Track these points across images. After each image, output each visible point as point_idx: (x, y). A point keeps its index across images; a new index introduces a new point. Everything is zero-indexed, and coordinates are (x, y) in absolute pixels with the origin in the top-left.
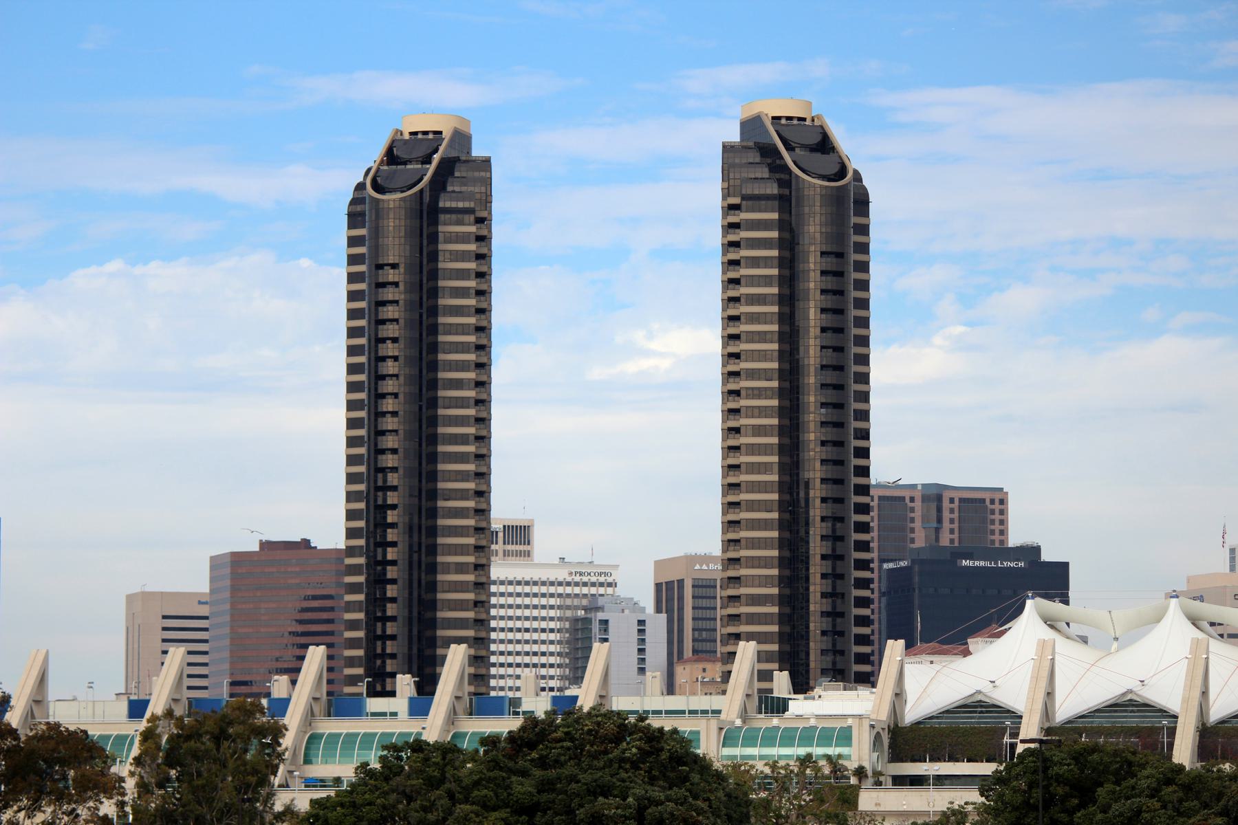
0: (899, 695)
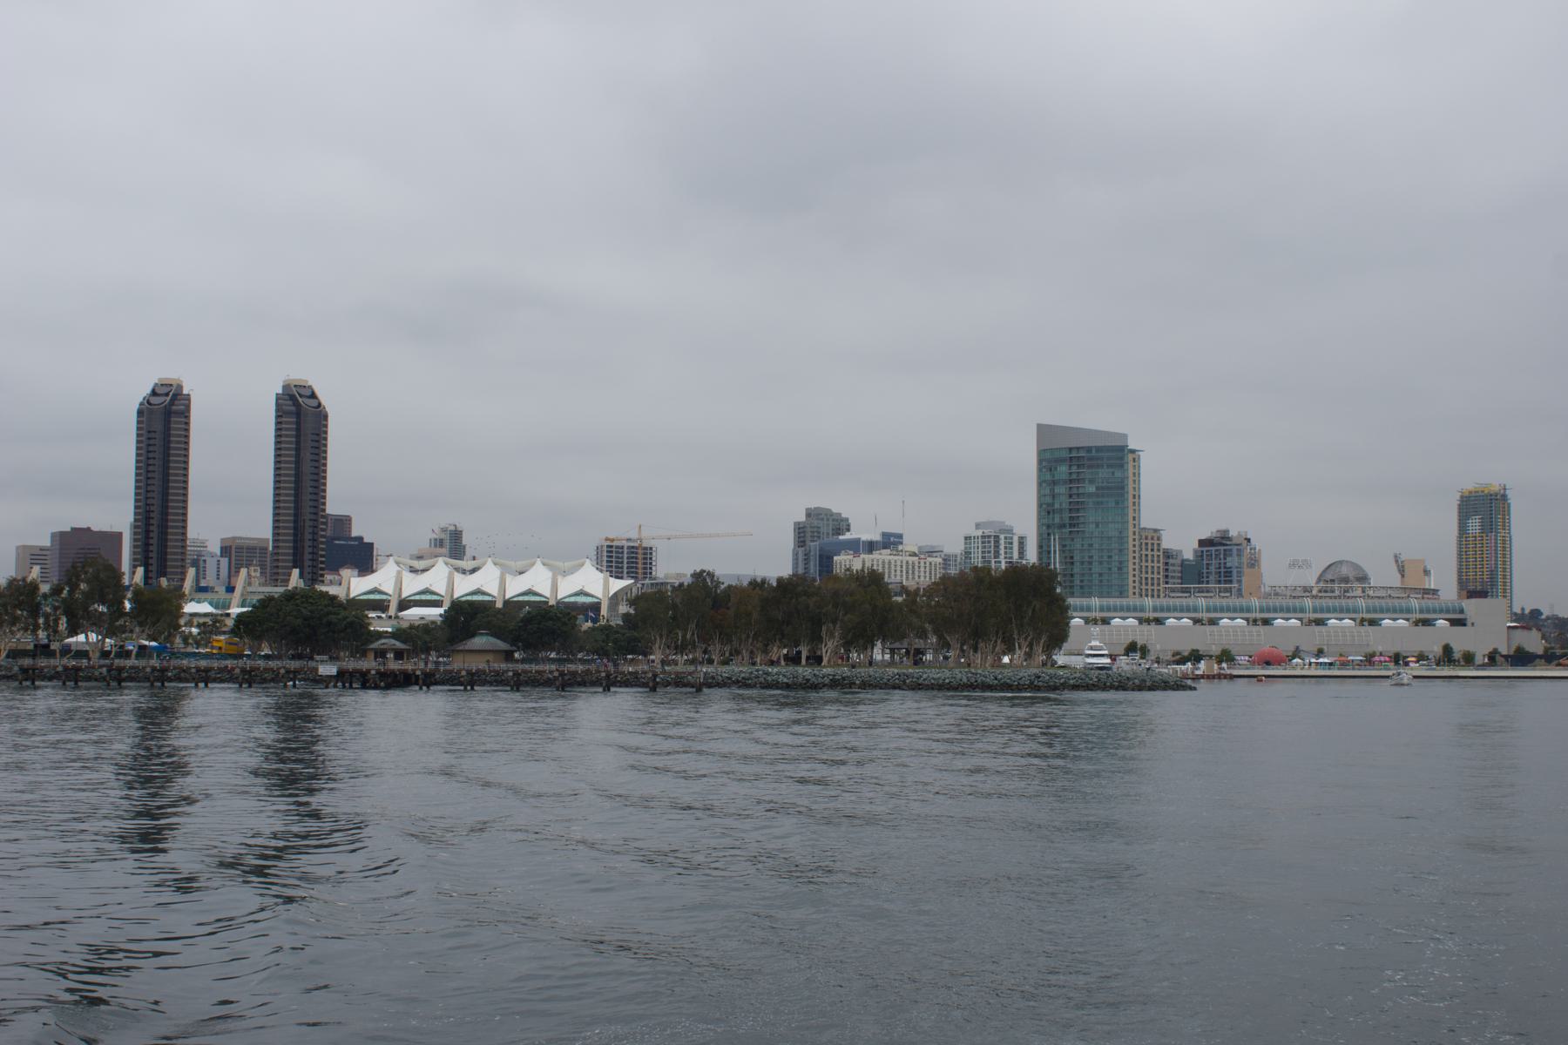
0: (349, 588)
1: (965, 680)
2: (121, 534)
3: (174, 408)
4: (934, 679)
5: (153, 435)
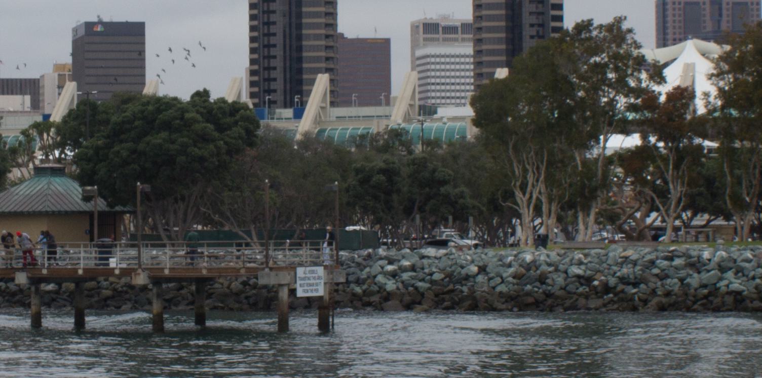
2: (385, 44)
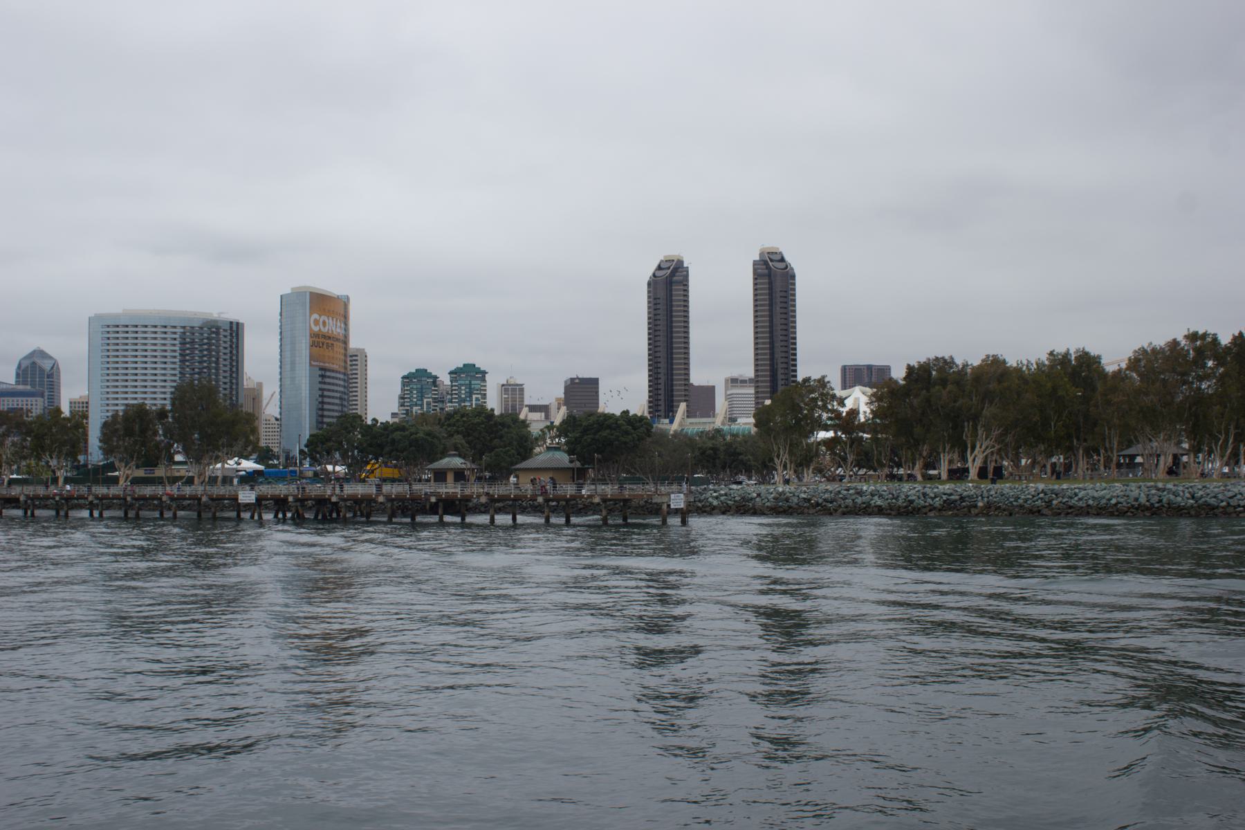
1: (1143, 500)
3: (675, 278)
4: (1094, 498)
5: (658, 301)
